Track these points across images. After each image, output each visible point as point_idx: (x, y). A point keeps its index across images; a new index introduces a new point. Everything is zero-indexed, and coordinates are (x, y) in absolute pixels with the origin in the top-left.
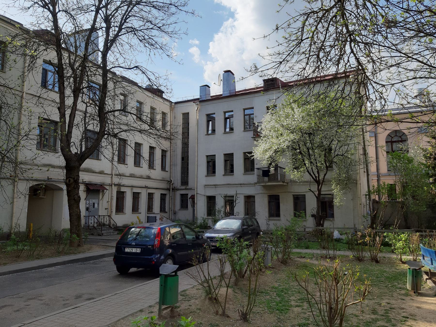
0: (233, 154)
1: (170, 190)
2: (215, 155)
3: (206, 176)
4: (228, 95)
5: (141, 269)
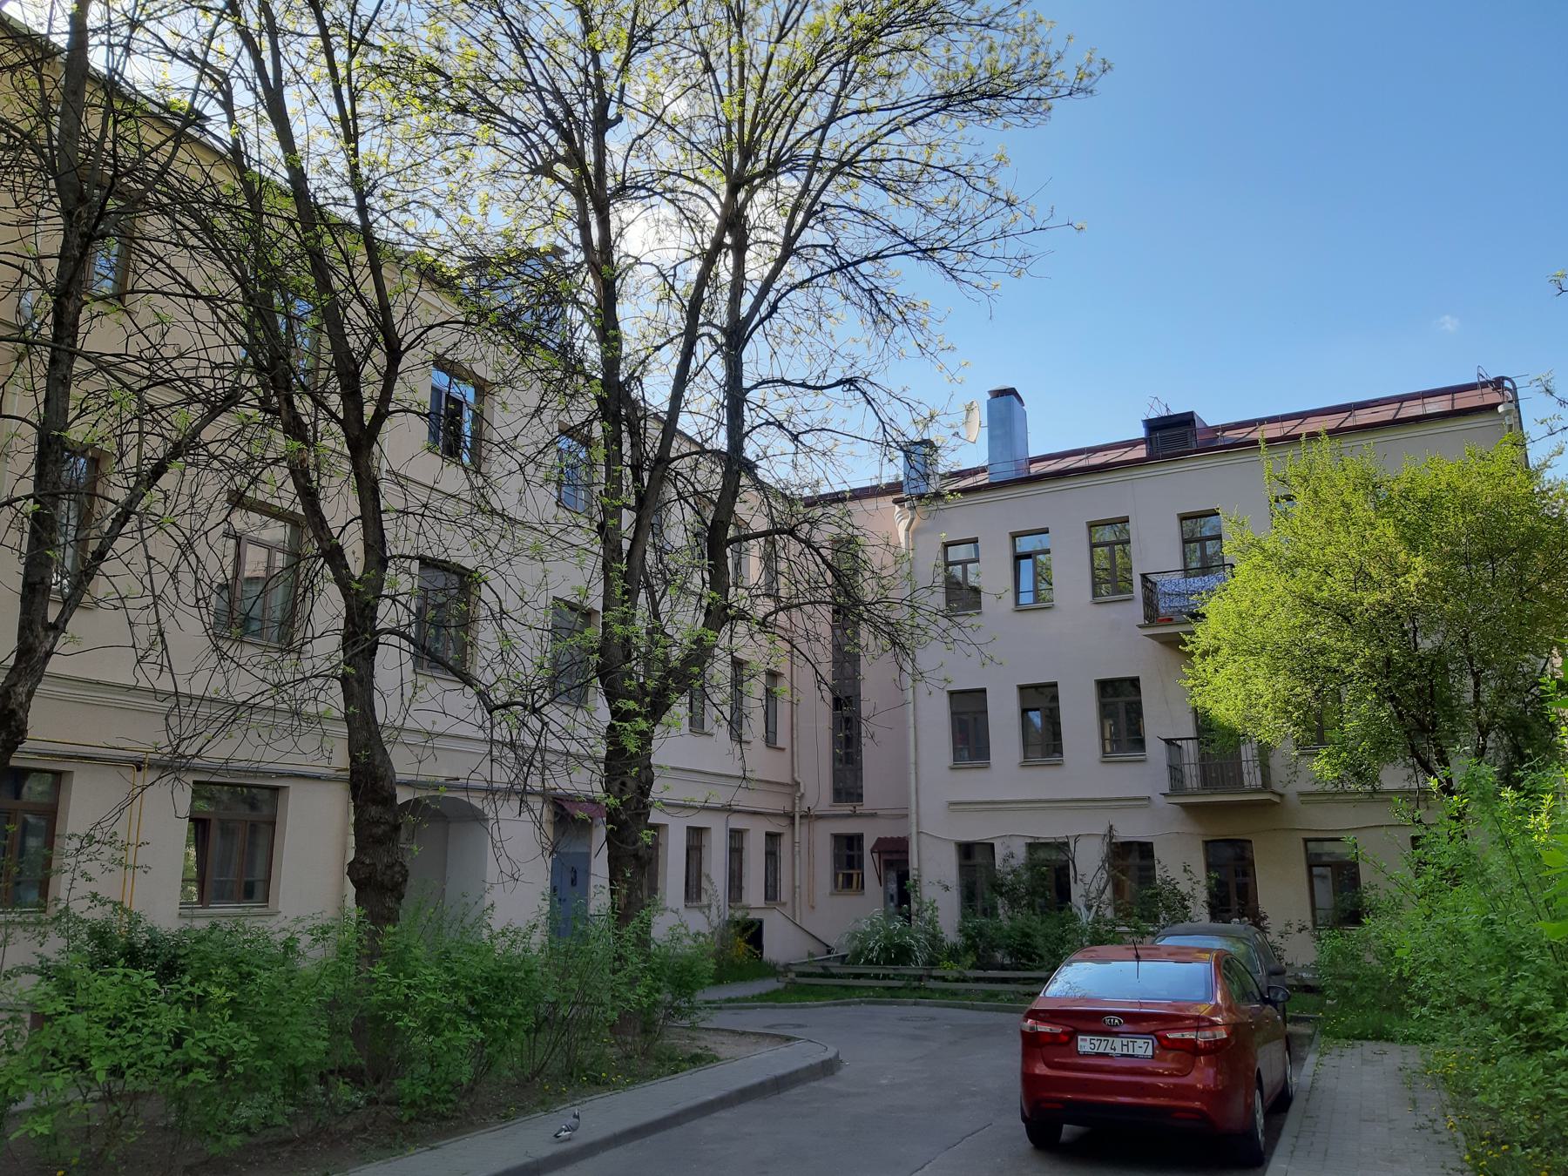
0: (984, 691)
1: (793, 818)
4: (1012, 476)
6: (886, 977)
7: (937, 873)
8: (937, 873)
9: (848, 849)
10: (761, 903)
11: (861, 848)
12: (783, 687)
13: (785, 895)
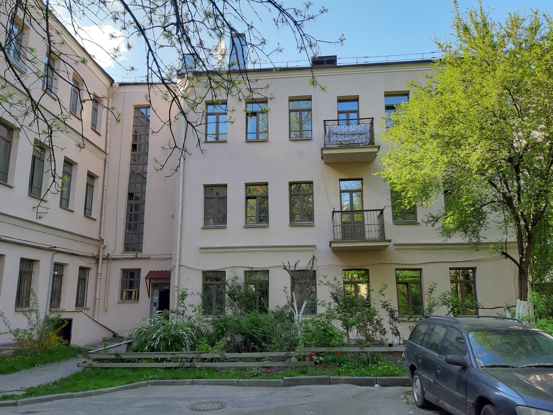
1: (98, 260)
2: (225, 186)
3: (203, 228)
5: (541, 389)
6: (162, 360)
7: (188, 286)
8: (188, 286)
9: (130, 279)
10: (73, 308)
11: (139, 277)
12: (98, 184)
13: (89, 302)
